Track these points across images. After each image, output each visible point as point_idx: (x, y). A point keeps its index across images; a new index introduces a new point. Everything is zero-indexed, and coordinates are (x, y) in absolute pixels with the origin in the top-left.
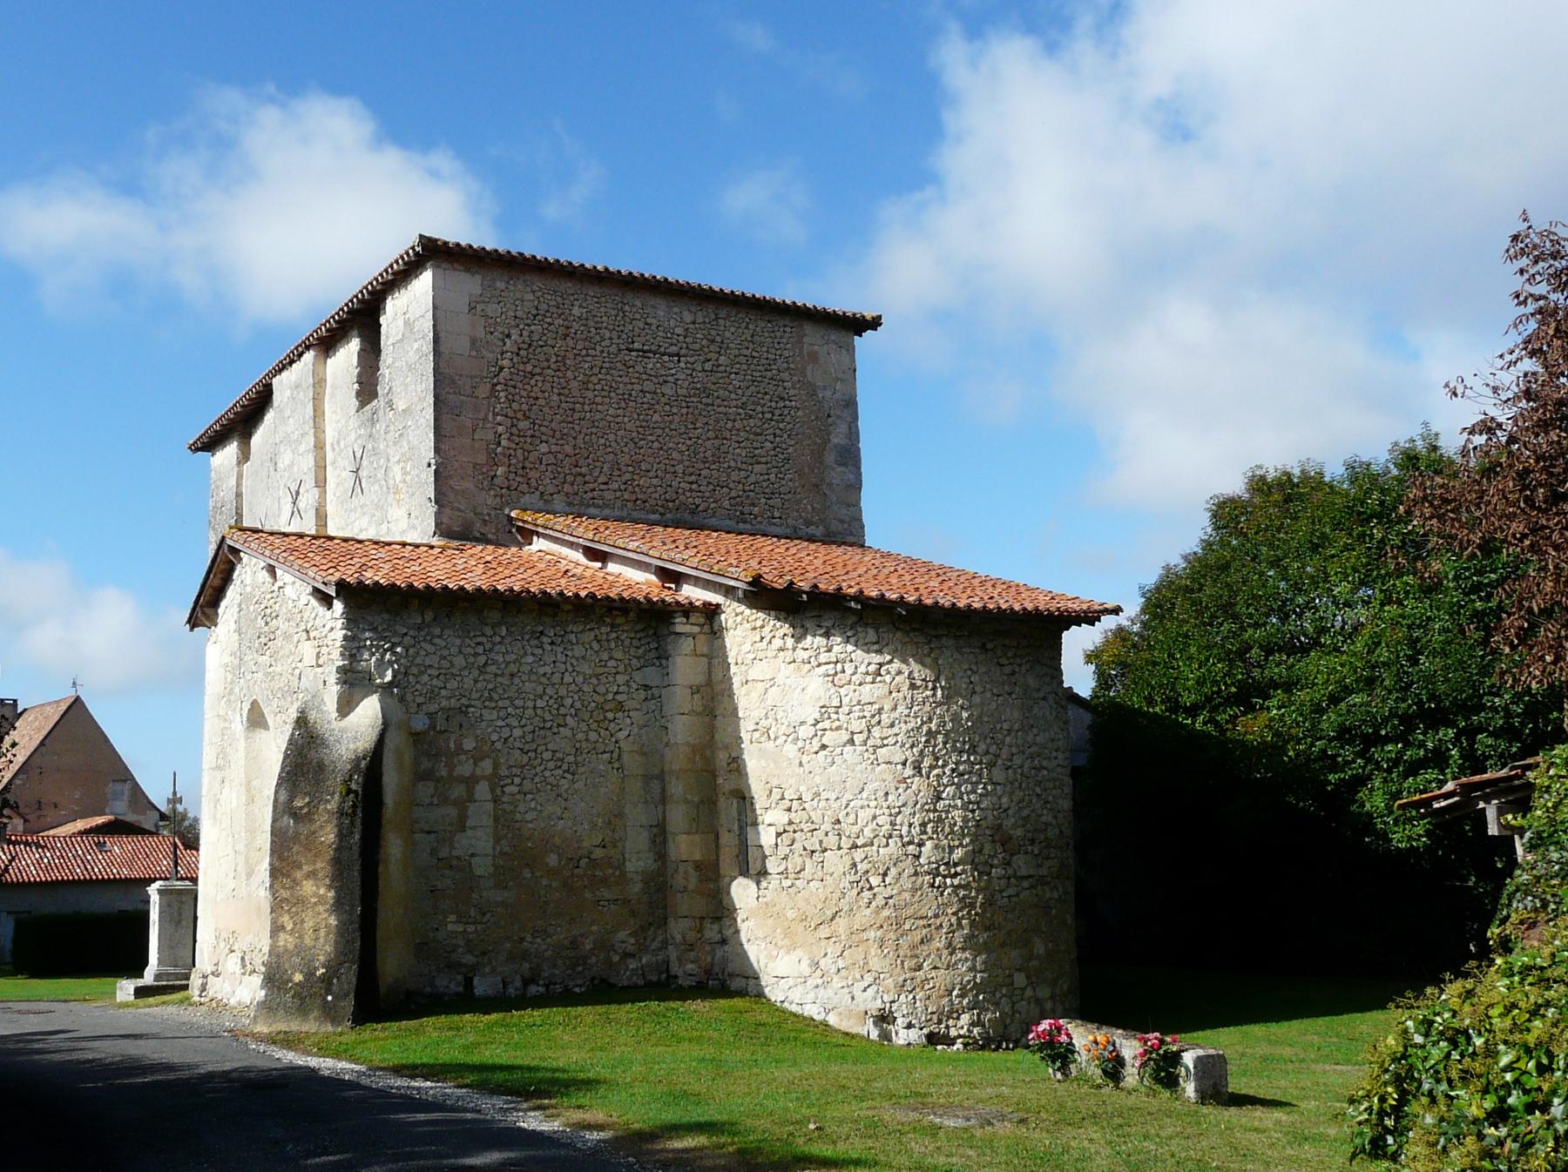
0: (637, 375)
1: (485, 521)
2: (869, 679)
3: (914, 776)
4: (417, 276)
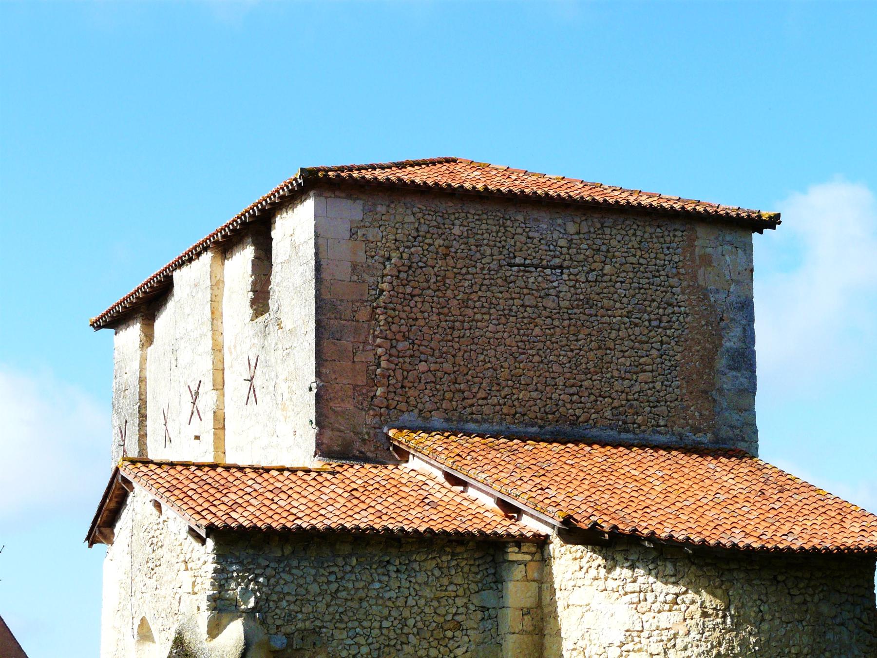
1: (364, 440)
2: (667, 607)
4: (301, 202)
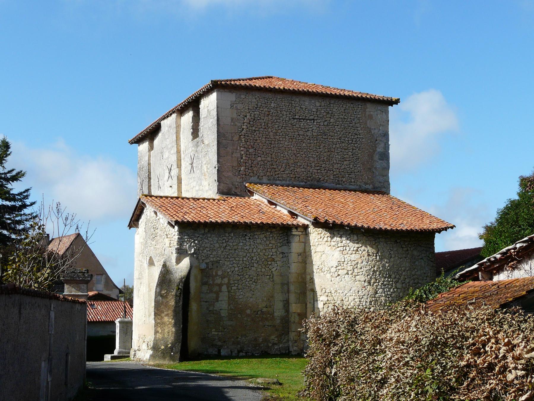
0: (296, 129)
2: (354, 252)
3: (368, 285)
4: (211, 94)
